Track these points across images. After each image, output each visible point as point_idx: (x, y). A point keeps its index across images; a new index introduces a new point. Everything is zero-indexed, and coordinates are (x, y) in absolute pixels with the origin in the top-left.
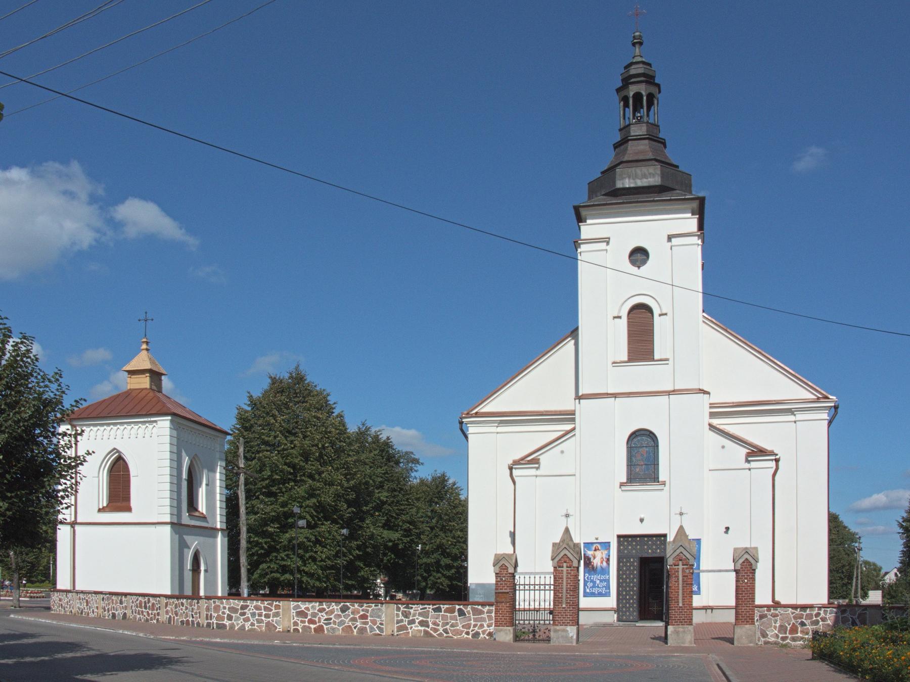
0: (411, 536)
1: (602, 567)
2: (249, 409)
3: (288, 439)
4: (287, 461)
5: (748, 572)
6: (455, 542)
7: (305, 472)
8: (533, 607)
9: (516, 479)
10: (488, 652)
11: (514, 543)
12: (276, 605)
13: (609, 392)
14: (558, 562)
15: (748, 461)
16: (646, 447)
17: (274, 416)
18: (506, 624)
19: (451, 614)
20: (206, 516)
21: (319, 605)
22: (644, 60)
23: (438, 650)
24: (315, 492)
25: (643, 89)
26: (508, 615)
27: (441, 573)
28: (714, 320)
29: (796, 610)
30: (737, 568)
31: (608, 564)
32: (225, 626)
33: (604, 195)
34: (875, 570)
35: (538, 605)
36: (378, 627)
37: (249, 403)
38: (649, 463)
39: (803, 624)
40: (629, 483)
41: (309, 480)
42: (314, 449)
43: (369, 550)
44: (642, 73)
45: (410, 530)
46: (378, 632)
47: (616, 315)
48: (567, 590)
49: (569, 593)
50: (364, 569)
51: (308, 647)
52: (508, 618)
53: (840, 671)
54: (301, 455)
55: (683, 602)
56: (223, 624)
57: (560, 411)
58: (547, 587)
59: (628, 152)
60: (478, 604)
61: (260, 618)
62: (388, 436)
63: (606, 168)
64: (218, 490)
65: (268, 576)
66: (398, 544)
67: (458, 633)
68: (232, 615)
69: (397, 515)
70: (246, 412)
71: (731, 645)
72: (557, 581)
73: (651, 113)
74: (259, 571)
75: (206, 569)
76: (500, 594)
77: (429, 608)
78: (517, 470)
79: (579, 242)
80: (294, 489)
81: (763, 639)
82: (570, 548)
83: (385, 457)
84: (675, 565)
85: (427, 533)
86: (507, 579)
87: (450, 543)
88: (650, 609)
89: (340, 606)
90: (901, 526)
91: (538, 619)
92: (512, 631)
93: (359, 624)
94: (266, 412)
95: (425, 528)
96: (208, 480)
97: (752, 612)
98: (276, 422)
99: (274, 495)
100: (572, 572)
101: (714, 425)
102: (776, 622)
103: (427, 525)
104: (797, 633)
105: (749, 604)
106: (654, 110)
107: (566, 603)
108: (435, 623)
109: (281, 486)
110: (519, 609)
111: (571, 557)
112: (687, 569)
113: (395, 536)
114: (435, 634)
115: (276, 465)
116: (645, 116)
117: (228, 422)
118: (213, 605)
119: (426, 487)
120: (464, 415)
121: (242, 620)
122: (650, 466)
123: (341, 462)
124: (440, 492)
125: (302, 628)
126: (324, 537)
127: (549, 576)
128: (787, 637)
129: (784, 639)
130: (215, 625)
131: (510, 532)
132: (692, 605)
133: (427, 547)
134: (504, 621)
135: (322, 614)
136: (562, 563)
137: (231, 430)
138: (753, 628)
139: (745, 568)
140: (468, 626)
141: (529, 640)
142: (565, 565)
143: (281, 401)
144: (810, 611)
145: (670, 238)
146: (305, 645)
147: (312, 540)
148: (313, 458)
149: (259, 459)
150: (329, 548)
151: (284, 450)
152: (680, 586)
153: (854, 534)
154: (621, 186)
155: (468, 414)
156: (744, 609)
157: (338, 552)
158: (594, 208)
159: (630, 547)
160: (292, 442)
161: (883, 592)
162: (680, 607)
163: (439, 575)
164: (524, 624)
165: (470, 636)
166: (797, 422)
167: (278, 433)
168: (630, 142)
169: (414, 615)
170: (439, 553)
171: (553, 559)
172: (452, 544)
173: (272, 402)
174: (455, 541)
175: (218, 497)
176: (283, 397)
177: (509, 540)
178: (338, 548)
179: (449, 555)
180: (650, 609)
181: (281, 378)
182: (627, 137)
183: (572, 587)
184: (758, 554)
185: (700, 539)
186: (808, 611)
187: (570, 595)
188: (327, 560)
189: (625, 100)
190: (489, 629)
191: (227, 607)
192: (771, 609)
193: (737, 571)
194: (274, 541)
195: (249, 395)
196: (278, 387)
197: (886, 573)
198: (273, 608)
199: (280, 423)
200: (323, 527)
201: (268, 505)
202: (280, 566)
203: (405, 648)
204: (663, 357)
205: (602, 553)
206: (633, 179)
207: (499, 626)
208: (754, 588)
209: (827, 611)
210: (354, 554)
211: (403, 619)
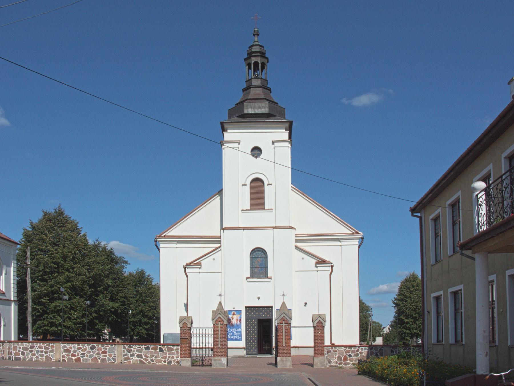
0: (125, 306)
1: (237, 324)
2: (31, 230)
3: (54, 248)
4: (54, 261)
6: (150, 309)
7: (64, 268)
9: (188, 274)
10: (178, 372)
11: (187, 310)
12: (52, 346)
13: (240, 226)
15: (316, 267)
16: (261, 257)
17: (45, 234)
20: (5, 293)
21: (78, 346)
22: (260, 44)
23: (149, 371)
24: (70, 279)
25: (259, 60)
26: (188, 351)
28: (297, 189)
29: (347, 348)
30: (314, 325)
31: (241, 322)
32: (20, 358)
33: (237, 117)
34: (378, 326)
35: (205, 345)
36: (113, 358)
37: (31, 226)
38: (262, 267)
39: (350, 356)
40: (251, 277)
41: (66, 272)
42: (69, 254)
43: (101, 313)
44: (258, 51)
45: (124, 302)
46: (113, 361)
47: (244, 184)
48: (221, 337)
49: (222, 339)
50: (99, 324)
51: (73, 371)
53: (376, 381)
54: (62, 257)
55: (285, 344)
56: (19, 358)
57: (212, 236)
58: (210, 335)
59: (250, 94)
61: (42, 353)
62: (112, 247)
63: (238, 102)
64: (12, 277)
65: (42, 329)
66: (118, 310)
67: (159, 361)
68: (25, 352)
70: (29, 231)
71: (312, 368)
72: (215, 332)
73: (263, 73)
74: (36, 326)
75: (5, 324)
76: (183, 339)
77: (143, 347)
78: (188, 269)
79: (223, 142)
80: (58, 277)
81: (329, 364)
82: (222, 313)
83: (110, 260)
84: (281, 324)
86: (187, 331)
87: (147, 309)
89: (90, 346)
90: (394, 303)
92: (190, 360)
93: (102, 357)
94: (41, 232)
95: (133, 301)
96: (6, 271)
98: (47, 238)
99: (46, 280)
100: (224, 327)
101: (298, 246)
102: (336, 354)
104: (347, 361)
105: (322, 345)
106: (265, 72)
107: (221, 344)
108: (146, 356)
109: (50, 275)
110: (194, 347)
111: (223, 319)
112: (287, 325)
113: (116, 305)
114: (146, 362)
115: (47, 263)
117: (18, 237)
118: (13, 346)
120: (157, 237)
121: (31, 355)
122: (263, 268)
123: (85, 262)
124: (141, 280)
125: (67, 359)
126: (75, 306)
127: (211, 329)
129: (340, 364)
130: (14, 358)
131: (185, 304)
132: (290, 345)
133: (134, 312)
135: (79, 351)
136: (218, 322)
137: (19, 242)
138: (324, 358)
139: (319, 325)
140: (165, 358)
141: (199, 366)
142: (219, 323)
143: (50, 225)
144: (354, 349)
145: (273, 142)
146: (71, 369)
147: (68, 307)
148: (69, 259)
149: (37, 259)
150: (78, 312)
151: (52, 254)
152: (284, 335)
153: (368, 307)
155: (160, 236)
157: (83, 314)
158: (232, 123)
159: (252, 313)
160: (56, 250)
161: (383, 338)
162: (284, 347)
163: (141, 328)
166: (342, 246)
167: (48, 244)
168: (252, 88)
169: (134, 351)
171: (213, 320)
172: (148, 310)
173: (45, 226)
174: (150, 308)
175: (12, 281)
176: (51, 224)
177: (184, 308)
178: (84, 312)
179: (146, 316)
181: (50, 212)
182: (250, 85)
185: (291, 309)
186: (353, 349)
188: (77, 319)
189: (249, 65)
190: (177, 359)
191: (22, 347)
193: (314, 327)
194: (46, 307)
195: (30, 221)
196: (48, 217)
197: (384, 328)
198: (50, 348)
199: (49, 238)
200: (75, 299)
201: (42, 286)
202: (50, 322)
203: (130, 371)
205: (237, 317)
206: (254, 109)
208: (324, 336)
209: (363, 348)
210: (94, 316)
211: (127, 354)
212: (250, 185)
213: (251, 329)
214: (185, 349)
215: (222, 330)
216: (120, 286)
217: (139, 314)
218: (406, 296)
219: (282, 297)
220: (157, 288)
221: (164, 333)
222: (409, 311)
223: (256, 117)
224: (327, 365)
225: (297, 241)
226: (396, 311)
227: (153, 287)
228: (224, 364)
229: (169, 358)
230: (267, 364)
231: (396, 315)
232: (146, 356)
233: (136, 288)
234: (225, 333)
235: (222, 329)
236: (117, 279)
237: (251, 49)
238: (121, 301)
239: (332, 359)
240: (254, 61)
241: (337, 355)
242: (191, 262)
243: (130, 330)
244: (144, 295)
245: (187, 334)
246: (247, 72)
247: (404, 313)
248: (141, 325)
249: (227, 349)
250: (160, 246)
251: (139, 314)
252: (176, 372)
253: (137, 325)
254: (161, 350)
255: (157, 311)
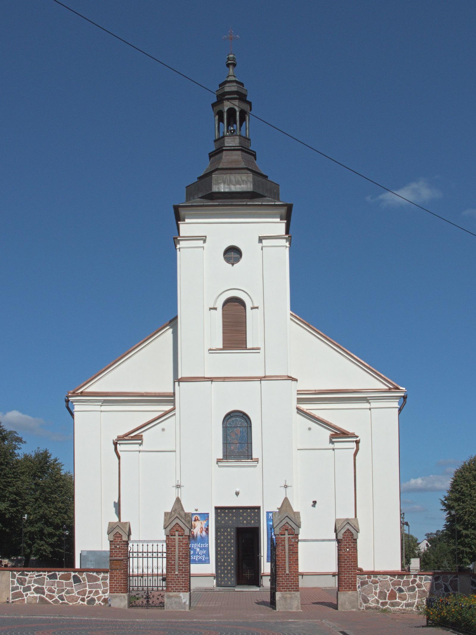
1: (201, 536)
5: (350, 541)
6: (57, 513)
8: (137, 573)
14: (170, 531)
15: (332, 442)
18: (121, 590)
19: (66, 581)
22: (237, 79)
26: (122, 582)
27: (44, 540)
29: (395, 578)
30: (339, 538)
33: (200, 198)
39: (400, 590)
40: (225, 460)
44: (235, 91)
47: (212, 307)
48: (179, 558)
49: (181, 561)
52: (122, 584)
57: (159, 393)
59: (222, 161)
60: (93, 571)
66: (5, 514)
67: (73, 599)
69: (4, 486)
72: (170, 548)
76: (115, 561)
77: (45, 575)
79: (178, 238)
82: (182, 517)
84: (281, 535)
85: (31, 504)
86: (121, 547)
87: (52, 513)
88: (244, 574)
90: (444, 504)
91: (151, 585)
92: (126, 598)
95: (30, 499)
97: (354, 579)
100: (184, 541)
102: (376, 588)
103: (32, 497)
104: (396, 599)
106: (246, 126)
107: (179, 570)
108: (50, 590)
112: (292, 538)
114: (50, 601)
116: (238, 130)
119: (30, 463)
120: (70, 394)
124: (42, 467)
127: (161, 544)
128: (386, 603)
129: (383, 604)
131: (115, 503)
134: (118, 588)
136: (174, 532)
139: (347, 538)
142: (177, 533)
144: (407, 578)
145: (261, 239)
152: (287, 554)
154: (217, 190)
155: (74, 393)
156: (347, 576)
159: (227, 518)
162: (287, 574)
163: (43, 542)
164: (138, 591)
165: (85, 603)
166: (372, 409)
168: (224, 152)
169: (30, 582)
170: (42, 522)
171: (165, 528)
172: (54, 515)
174: (57, 511)
177: (113, 510)
179: (51, 524)
180: (244, 574)
183: (184, 555)
184: (358, 524)
187: (182, 563)
189: (220, 114)
190: (104, 595)
192: (371, 577)
193: (339, 541)
204: (255, 346)
206: (228, 185)
207: (114, 593)
209: (422, 578)
211: (18, 587)
212: (223, 309)
213: (224, 544)
214: (119, 578)
216: (10, 475)
217: (40, 520)
218: (463, 494)
220: (68, 480)
221: (81, 551)
222: (469, 517)
223: (232, 198)
224: (361, 606)
225: (299, 401)
226: (448, 517)
227: (61, 479)
228: (185, 603)
229: (91, 594)
230: (256, 603)
231: (448, 524)
232: (50, 590)
233: (34, 479)
234: (186, 551)
236: (4, 464)
237: (224, 87)
238: (10, 499)
239: (369, 595)
240: (228, 107)
241: (378, 588)
242: (126, 434)
243: (25, 546)
244: (48, 490)
245: (121, 552)
246: (217, 126)
247: (461, 520)
248: (43, 538)
249: (190, 576)
250: (74, 409)
251: (40, 520)
252: (104, 619)
253: (36, 538)
254: (77, 580)
255: (68, 516)
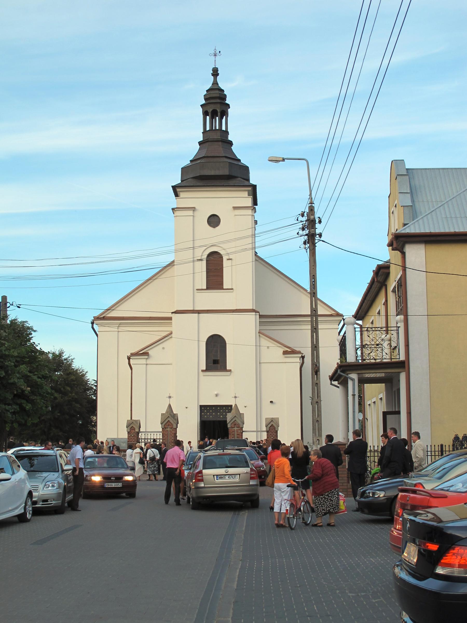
14: (164, 425)
49: (171, 444)
86: (135, 435)
100: (173, 431)
111: (172, 422)
112: (239, 430)
127: (159, 433)
171: (161, 424)
193: (267, 432)
215: (171, 435)
219: (234, 399)
221: (107, 438)
235: (171, 433)
240: (213, 109)
